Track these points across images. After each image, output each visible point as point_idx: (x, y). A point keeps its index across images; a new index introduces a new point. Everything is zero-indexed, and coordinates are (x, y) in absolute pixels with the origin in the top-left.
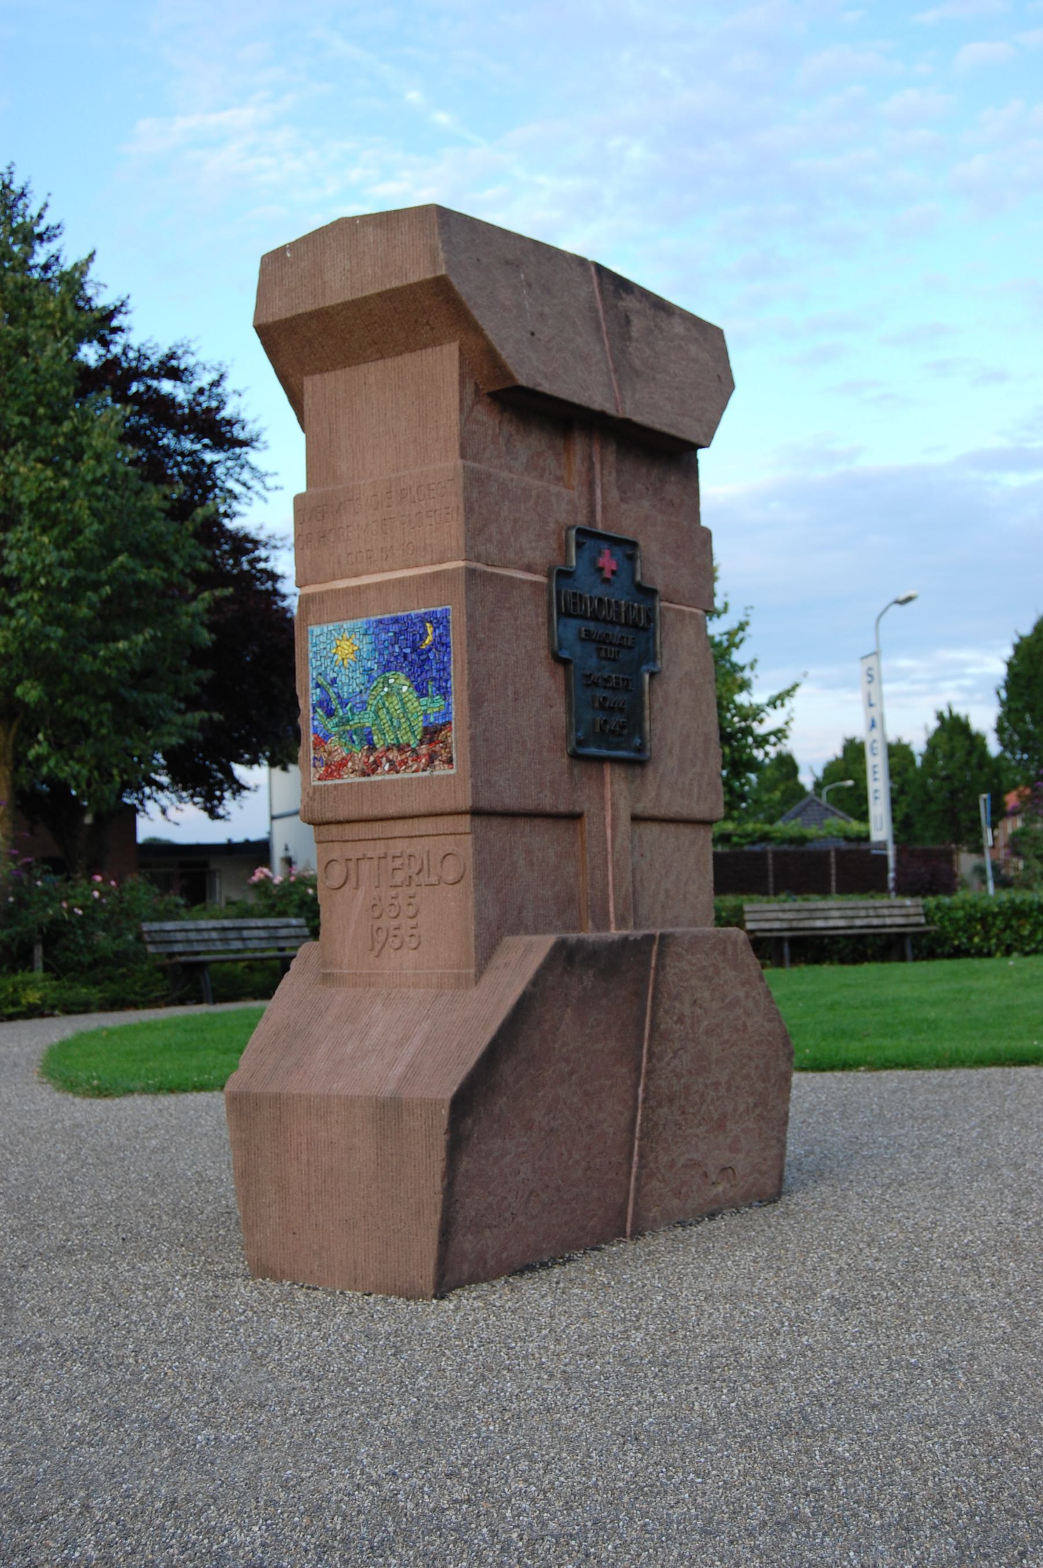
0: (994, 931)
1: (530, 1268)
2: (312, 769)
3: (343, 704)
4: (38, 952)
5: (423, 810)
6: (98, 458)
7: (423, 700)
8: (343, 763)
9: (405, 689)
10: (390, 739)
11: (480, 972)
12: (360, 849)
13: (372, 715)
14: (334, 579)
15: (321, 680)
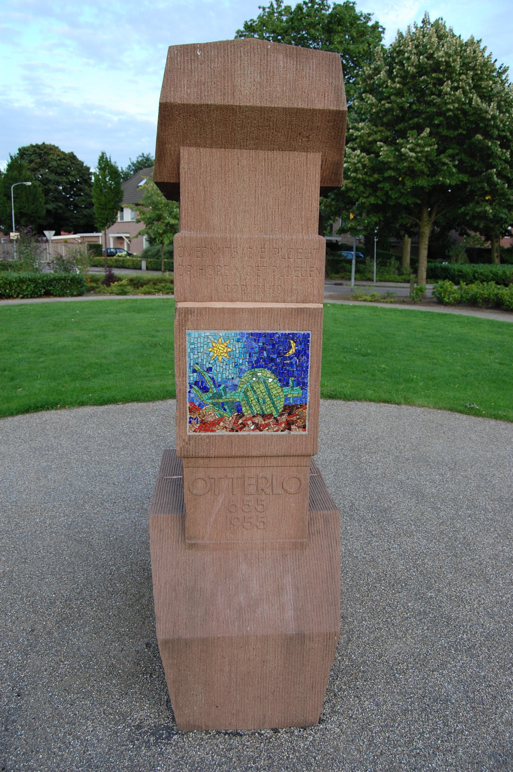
0: (14, 287)
2: (188, 424)
7: (285, 389)
9: (270, 380)
10: (256, 409)
13: (242, 394)
14: (212, 301)
15: (197, 367)
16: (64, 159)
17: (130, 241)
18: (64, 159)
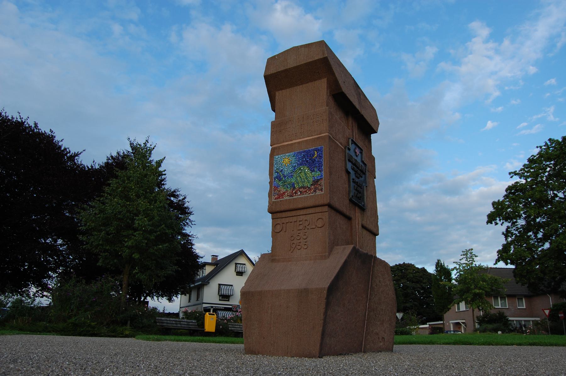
1: (341, 354)
3: (285, 177)
4: (129, 322)
5: (312, 205)
6: (160, 202)
7: (313, 173)
8: (284, 193)
11: (329, 254)
12: (287, 220)
16: (418, 272)
17: (466, 326)
18: (418, 272)
